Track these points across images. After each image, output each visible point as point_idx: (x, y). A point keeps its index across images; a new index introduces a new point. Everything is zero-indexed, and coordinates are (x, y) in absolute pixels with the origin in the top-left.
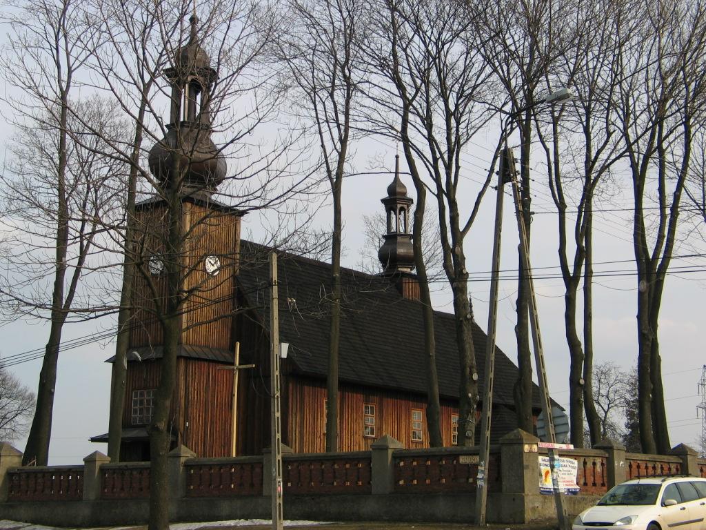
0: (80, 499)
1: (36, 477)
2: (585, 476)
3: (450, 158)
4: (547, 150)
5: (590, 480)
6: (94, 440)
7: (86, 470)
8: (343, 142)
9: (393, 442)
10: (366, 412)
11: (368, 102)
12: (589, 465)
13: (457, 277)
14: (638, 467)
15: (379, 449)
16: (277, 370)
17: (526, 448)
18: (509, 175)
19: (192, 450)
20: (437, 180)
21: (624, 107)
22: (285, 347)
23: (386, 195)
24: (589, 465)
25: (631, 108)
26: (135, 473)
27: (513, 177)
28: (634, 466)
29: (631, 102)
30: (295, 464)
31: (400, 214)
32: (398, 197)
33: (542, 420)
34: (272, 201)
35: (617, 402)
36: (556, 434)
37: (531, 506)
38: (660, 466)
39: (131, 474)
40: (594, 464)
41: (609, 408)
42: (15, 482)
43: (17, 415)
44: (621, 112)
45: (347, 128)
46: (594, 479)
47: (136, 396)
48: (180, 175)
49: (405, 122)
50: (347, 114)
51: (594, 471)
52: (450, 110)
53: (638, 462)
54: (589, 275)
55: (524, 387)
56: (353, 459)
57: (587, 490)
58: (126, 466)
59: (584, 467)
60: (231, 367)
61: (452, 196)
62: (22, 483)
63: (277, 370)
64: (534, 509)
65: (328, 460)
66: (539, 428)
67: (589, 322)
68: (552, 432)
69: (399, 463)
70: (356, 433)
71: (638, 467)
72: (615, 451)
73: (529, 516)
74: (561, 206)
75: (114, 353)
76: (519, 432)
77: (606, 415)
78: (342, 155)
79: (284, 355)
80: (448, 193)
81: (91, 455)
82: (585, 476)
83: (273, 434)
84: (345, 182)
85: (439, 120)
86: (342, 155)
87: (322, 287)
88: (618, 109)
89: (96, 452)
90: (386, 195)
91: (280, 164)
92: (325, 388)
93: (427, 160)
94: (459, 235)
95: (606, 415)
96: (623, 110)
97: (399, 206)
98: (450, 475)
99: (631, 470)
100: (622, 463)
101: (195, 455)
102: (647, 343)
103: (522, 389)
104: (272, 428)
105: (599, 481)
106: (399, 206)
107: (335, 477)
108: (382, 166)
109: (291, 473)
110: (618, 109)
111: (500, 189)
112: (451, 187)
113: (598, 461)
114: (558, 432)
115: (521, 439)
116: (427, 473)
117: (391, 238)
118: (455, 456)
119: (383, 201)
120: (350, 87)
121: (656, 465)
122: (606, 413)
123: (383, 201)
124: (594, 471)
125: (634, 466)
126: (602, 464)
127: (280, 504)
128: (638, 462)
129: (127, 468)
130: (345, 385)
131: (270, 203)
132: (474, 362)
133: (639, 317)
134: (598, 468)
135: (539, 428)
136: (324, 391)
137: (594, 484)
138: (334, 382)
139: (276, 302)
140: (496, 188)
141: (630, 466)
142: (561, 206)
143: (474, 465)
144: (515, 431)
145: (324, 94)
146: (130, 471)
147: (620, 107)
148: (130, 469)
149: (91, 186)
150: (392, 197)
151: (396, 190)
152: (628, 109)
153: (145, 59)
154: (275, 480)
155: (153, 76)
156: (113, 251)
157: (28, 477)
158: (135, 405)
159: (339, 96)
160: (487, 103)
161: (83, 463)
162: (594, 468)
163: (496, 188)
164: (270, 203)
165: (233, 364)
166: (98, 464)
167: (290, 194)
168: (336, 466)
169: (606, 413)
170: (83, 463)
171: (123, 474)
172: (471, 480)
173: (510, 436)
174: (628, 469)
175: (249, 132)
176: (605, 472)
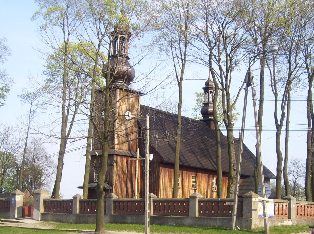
0: (72, 213)
1: (54, 203)
2: (278, 211)
3: (227, 75)
4: (270, 71)
5: (280, 212)
6: (79, 188)
7: (73, 201)
8: (183, 65)
9: (199, 195)
10: (193, 178)
11: (194, 48)
12: (281, 206)
13: (229, 126)
14: (301, 207)
15: (193, 198)
16: (148, 165)
17: (254, 200)
18: (250, 83)
19: (116, 195)
20: (222, 84)
21: (306, 51)
22: (152, 155)
23: (204, 86)
24: (281, 206)
25: (309, 52)
26: (93, 203)
27: (252, 84)
28: (300, 207)
29: (309, 49)
30: (158, 203)
31: (210, 94)
32: (209, 87)
33: (260, 188)
34: (148, 92)
35: (301, 175)
36: (266, 194)
37: (254, 223)
38: (310, 206)
39: (92, 203)
40: (283, 206)
41: (297, 177)
42: (46, 204)
43: (52, 173)
44: (305, 54)
45: (185, 60)
46: (282, 212)
47: (96, 170)
48: (110, 81)
49: (210, 59)
50: (185, 55)
51: (282, 209)
52: (228, 54)
53: (301, 205)
54: (279, 130)
55: (258, 171)
56: (182, 201)
57: (279, 217)
58: (90, 200)
59: (278, 207)
60: (135, 159)
61: (228, 90)
62: (49, 205)
63: (148, 165)
64: (255, 225)
65: (172, 201)
66: (259, 192)
67: (287, 144)
68: (264, 193)
69: (201, 204)
70: (188, 187)
71: (301, 207)
72: (291, 200)
73: (253, 227)
74: (276, 95)
75: (86, 153)
76: (251, 193)
77: (296, 180)
78: (183, 71)
79: (151, 159)
80: (226, 89)
81: (76, 195)
82: (278, 211)
83: (146, 192)
84: (184, 82)
85: (223, 58)
86: (183, 71)
87: (167, 131)
88: (304, 52)
89: (77, 194)
90: (204, 86)
91: (151, 76)
92: (173, 169)
93: (218, 74)
94: (230, 107)
95: (296, 180)
96: (305, 52)
97: (210, 91)
98: (222, 210)
99: (298, 208)
100: (294, 205)
101: (118, 197)
102: (311, 153)
103: (258, 171)
104: (146, 190)
105: (284, 213)
106: (210, 91)
107: (174, 209)
108: (198, 76)
109: (156, 206)
110: (304, 52)
111: (246, 90)
112: (227, 86)
113: (284, 204)
114: (267, 193)
115: (252, 196)
116: (212, 208)
117: (206, 104)
118: (224, 201)
119: (203, 88)
120: (187, 42)
121: (309, 206)
122: (296, 179)
123: (203, 88)
124: (282, 209)
125: (300, 207)
126: (286, 206)
127: (148, 221)
128: (301, 205)
129: (90, 201)
130: (184, 167)
131: (147, 93)
132: (235, 162)
133: (307, 142)
134: (284, 207)
135: (259, 192)
136: (173, 170)
137: (282, 214)
138: (177, 167)
139: (148, 137)
140: (245, 89)
141: (298, 206)
142: (276, 95)
143: (232, 206)
144: (249, 192)
145: (176, 44)
146: (91, 203)
147: (304, 51)
148: (91, 202)
149: (80, 81)
150: (207, 87)
151: (209, 84)
152: (308, 52)
153: (100, 29)
154: (146, 211)
155: (103, 36)
156: (80, 114)
157: (51, 203)
158: (96, 174)
159: (182, 46)
160: (247, 49)
161: (72, 198)
162: (282, 207)
163: (245, 89)
164: (147, 93)
165: (136, 158)
166: (78, 199)
167: (156, 89)
168: (175, 204)
169: (296, 179)
170: (72, 198)
171: (88, 204)
172: (230, 212)
173: (247, 194)
174: (297, 208)
175: (138, 63)
176: (309, 186)
